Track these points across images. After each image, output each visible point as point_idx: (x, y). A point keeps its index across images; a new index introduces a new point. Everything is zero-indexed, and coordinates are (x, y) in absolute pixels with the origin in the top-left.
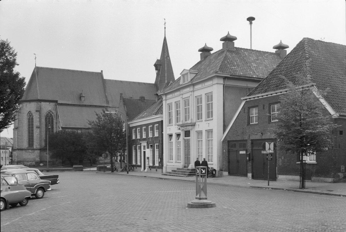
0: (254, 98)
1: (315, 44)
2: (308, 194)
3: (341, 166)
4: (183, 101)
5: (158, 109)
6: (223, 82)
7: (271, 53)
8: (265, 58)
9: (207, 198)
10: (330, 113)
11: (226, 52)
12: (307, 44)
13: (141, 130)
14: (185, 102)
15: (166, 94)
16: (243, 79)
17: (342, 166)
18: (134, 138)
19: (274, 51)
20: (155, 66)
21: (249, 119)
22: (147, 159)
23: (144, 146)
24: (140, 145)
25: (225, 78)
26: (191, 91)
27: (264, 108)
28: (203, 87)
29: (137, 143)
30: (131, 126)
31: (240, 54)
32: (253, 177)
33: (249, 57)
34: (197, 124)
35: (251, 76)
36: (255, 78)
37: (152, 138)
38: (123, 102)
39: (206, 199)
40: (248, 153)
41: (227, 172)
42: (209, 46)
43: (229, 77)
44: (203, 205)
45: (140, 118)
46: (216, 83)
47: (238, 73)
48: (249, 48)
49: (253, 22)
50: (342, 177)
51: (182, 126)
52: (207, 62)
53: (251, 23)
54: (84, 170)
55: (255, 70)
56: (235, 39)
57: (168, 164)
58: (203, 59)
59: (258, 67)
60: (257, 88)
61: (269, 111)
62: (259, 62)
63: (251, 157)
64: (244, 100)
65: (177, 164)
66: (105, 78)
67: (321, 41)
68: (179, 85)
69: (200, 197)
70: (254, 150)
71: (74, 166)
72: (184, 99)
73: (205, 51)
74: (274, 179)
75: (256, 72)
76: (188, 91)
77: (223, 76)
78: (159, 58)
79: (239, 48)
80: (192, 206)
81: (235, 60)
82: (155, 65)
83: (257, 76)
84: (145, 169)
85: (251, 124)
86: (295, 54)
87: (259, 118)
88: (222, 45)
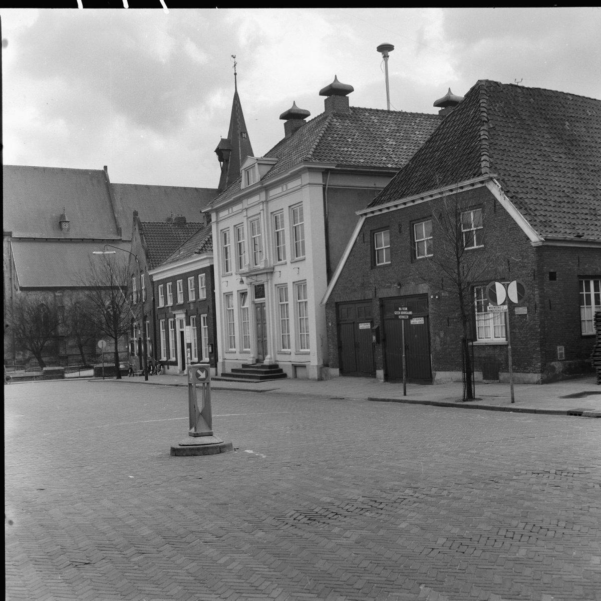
0: (380, 210)
1: (502, 91)
2: (493, 412)
3: (557, 349)
4: (249, 223)
5: (204, 242)
6: (323, 179)
7: (428, 115)
8: (415, 127)
9: (212, 432)
10: (527, 236)
11: (330, 118)
12: (486, 93)
13: (165, 288)
14: (253, 226)
15: (217, 211)
16: (361, 172)
17: (558, 347)
18: (161, 305)
19: (436, 111)
20: (218, 154)
21: (374, 255)
22: (188, 348)
23: (181, 321)
24: (172, 319)
25: (325, 172)
26: (263, 202)
27: (400, 232)
28: (285, 193)
29: (168, 315)
30: (155, 279)
31: (362, 121)
32: (388, 378)
33: (381, 127)
34: (277, 269)
35: (381, 165)
36: (392, 168)
37: (194, 302)
38: (139, 229)
39: (211, 434)
40: (375, 327)
41: (338, 369)
42: (301, 106)
43: (334, 169)
44: (202, 448)
45: (170, 263)
46: (308, 182)
47: (354, 160)
48: (386, 108)
49: (390, 53)
50: (561, 370)
51: (248, 275)
52: (295, 140)
53: (386, 57)
54: (66, 375)
55: (392, 153)
56: (350, 90)
57: (227, 356)
58: (290, 135)
59: (399, 145)
60: (386, 189)
61: (411, 236)
62: (403, 136)
63: (382, 335)
64: (362, 215)
65: (245, 356)
66: (112, 181)
67: (517, 86)
68: (241, 190)
69: (195, 431)
70: (388, 319)
71: (44, 369)
72: (250, 219)
73: (294, 117)
74: (427, 379)
75: (393, 156)
76: (257, 203)
77: (321, 169)
78: (226, 137)
79: (359, 108)
80: (176, 452)
81: (349, 133)
82: (218, 151)
83: (396, 164)
84: (184, 368)
85: (378, 265)
86: (461, 114)
87: (392, 252)
88: (324, 103)
